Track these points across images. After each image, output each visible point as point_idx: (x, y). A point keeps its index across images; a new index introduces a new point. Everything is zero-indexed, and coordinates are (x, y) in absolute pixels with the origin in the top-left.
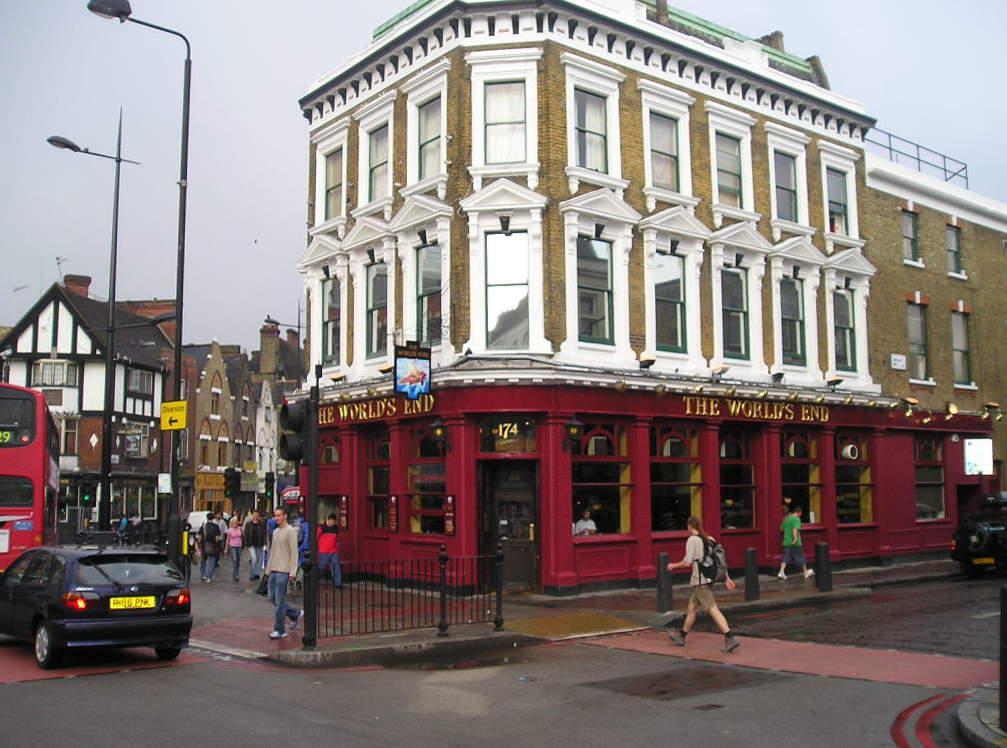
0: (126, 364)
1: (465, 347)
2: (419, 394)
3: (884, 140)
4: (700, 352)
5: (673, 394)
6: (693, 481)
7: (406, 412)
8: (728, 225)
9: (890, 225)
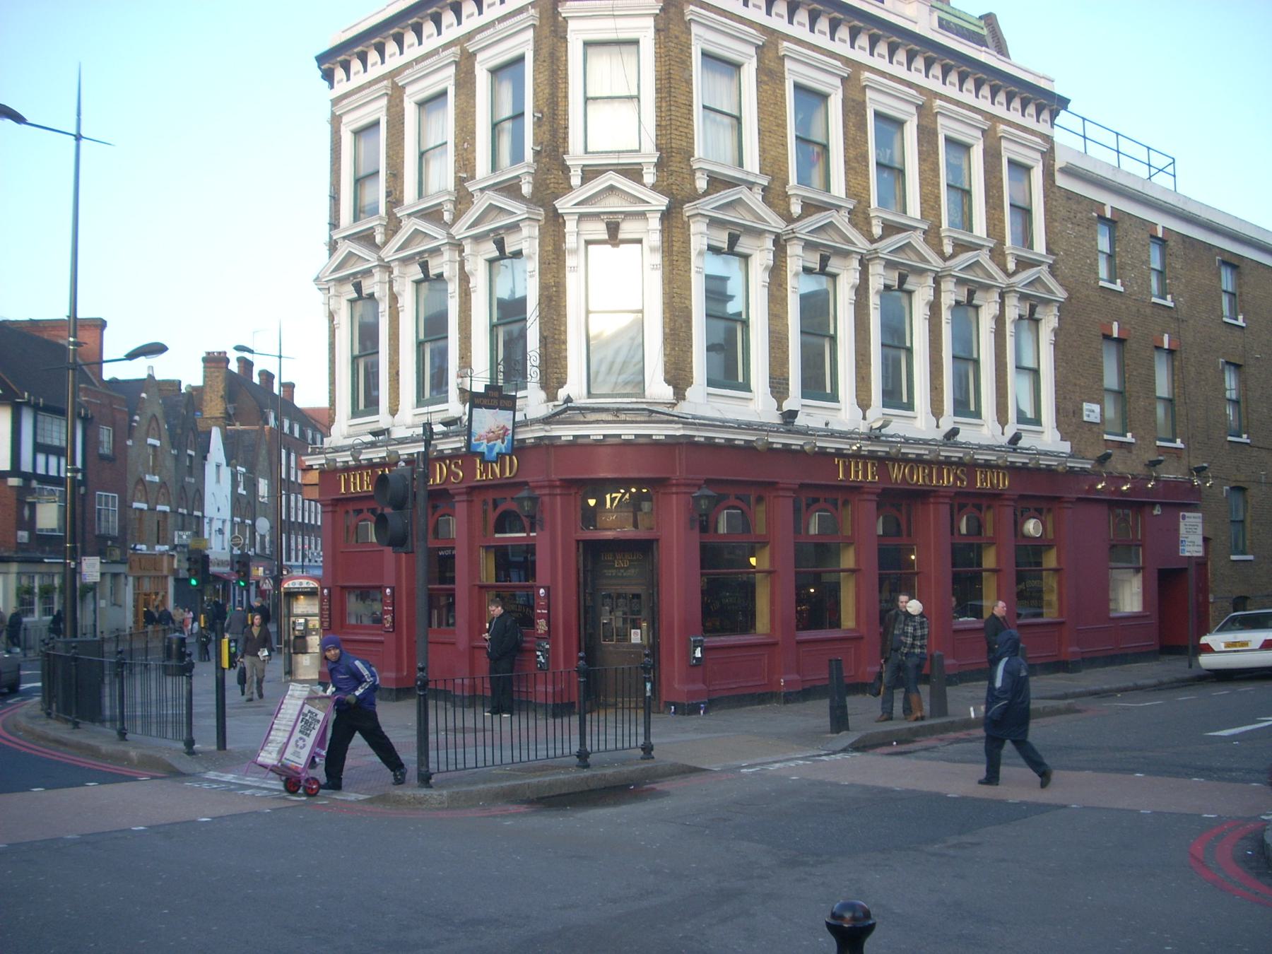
0: (36, 408)
1: (562, 394)
2: (498, 454)
3: (1077, 125)
4: (855, 401)
5: (823, 453)
6: (843, 566)
7: (478, 477)
8: (889, 236)
9: (1083, 237)
